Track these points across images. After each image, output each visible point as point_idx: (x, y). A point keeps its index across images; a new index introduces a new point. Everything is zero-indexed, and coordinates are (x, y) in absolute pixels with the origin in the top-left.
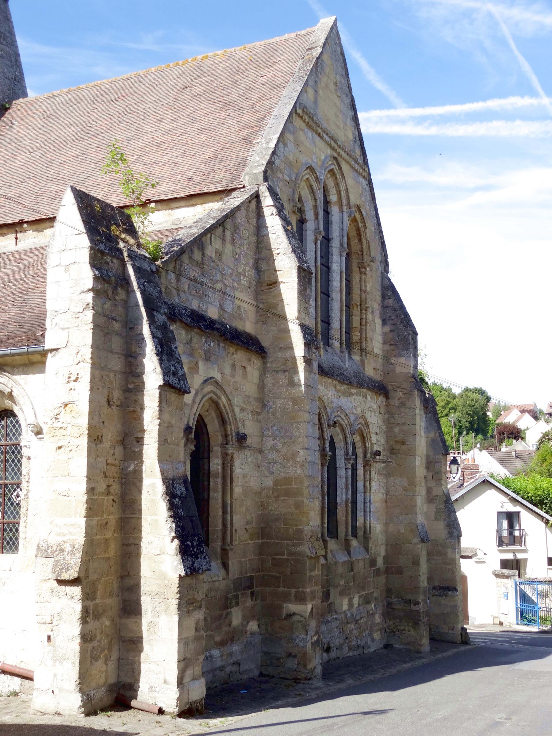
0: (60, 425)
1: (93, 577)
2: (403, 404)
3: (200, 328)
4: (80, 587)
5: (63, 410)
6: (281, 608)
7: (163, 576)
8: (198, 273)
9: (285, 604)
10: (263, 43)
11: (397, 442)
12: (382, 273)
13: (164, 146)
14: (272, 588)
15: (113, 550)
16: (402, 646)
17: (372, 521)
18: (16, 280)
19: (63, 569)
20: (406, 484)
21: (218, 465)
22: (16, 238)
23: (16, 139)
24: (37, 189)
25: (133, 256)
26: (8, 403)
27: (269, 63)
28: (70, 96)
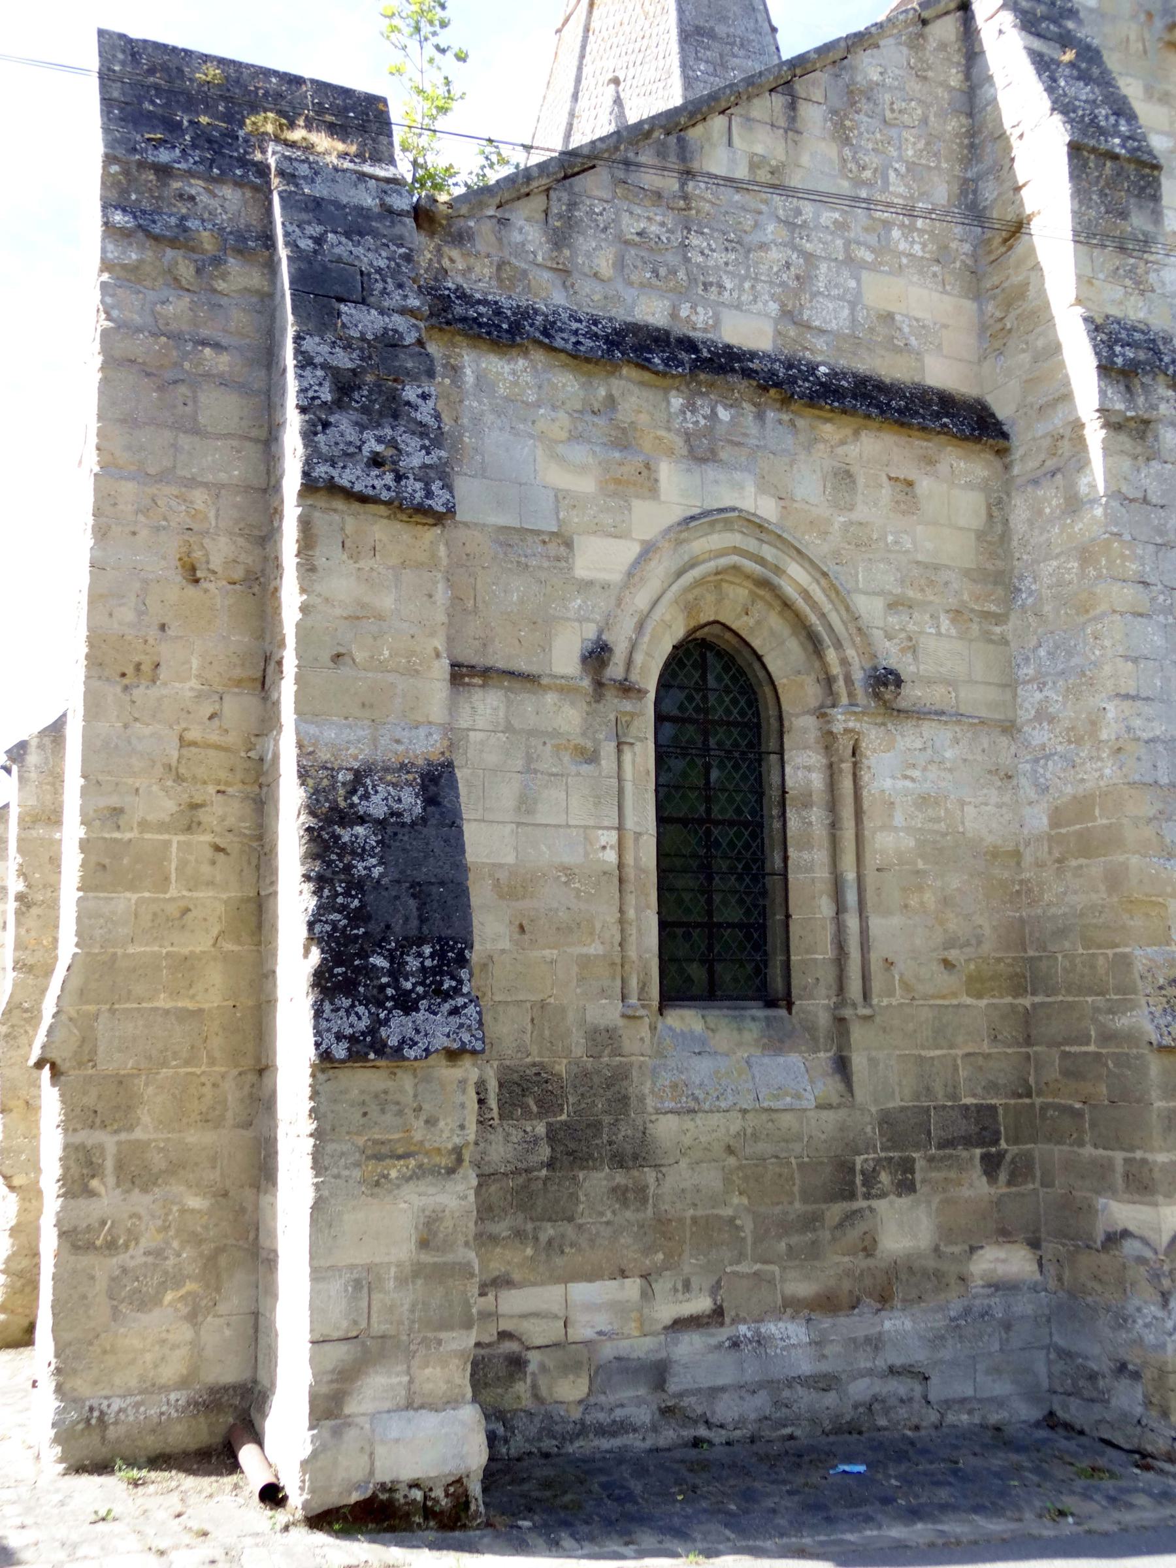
1: (111, 1062)
6: (1090, 1210)
8: (663, 224)
14: (1065, 1148)
21: (809, 769)
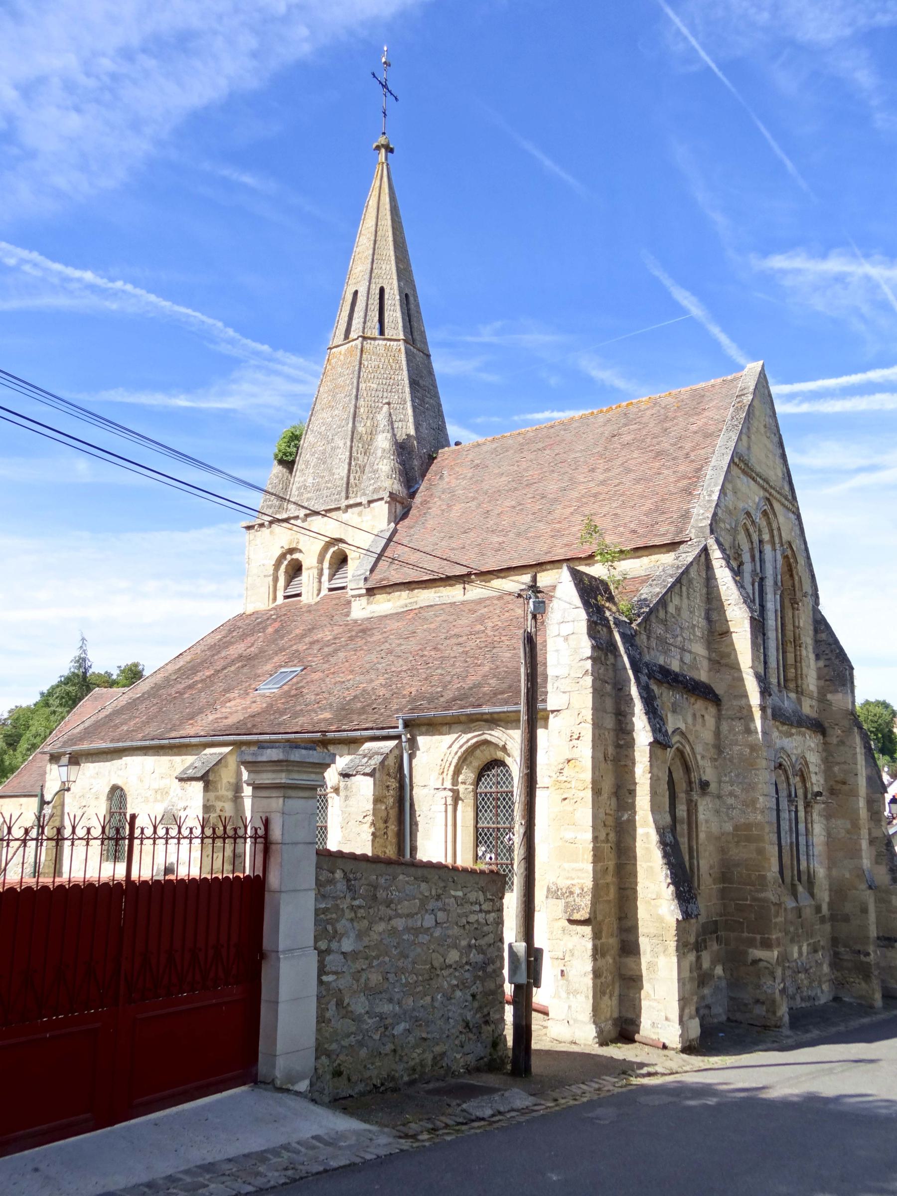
0: (564, 779)
2: (842, 743)
3: (669, 683)
4: (590, 927)
5: (567, 766)
6: (745, 953)
7: (660, 919)
9: (751, 950)
10: (688, 389)
11: (836, 781)
12: (813, 606)
13: (601, 497)
15: (612, 894)
16: (852, 1000)
17: (816, 865)
18: (478, 633)
19: (574, 909)
20: (849, 826)
21: (683, 811)
22: (464, 588)
23: (449, 488)
24: (479, 540)
25: (618, 623)
26: (500, 755)
27: (699, 410)
28: (495, 445)
